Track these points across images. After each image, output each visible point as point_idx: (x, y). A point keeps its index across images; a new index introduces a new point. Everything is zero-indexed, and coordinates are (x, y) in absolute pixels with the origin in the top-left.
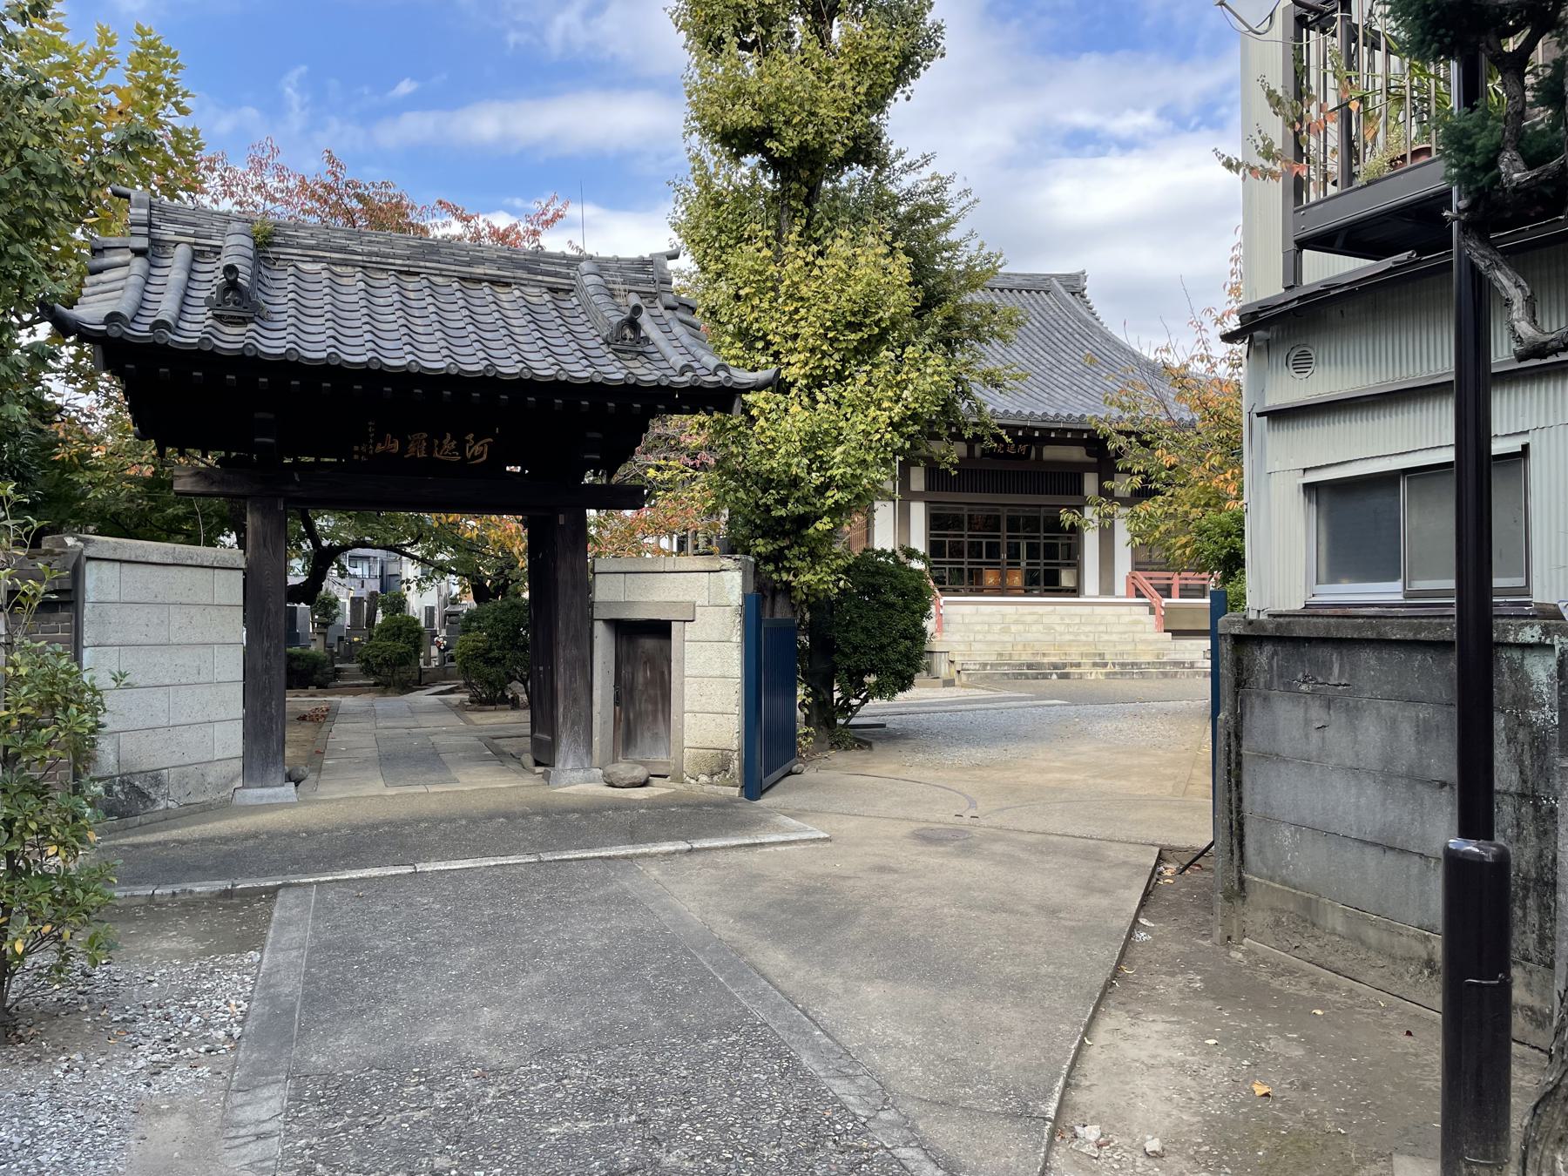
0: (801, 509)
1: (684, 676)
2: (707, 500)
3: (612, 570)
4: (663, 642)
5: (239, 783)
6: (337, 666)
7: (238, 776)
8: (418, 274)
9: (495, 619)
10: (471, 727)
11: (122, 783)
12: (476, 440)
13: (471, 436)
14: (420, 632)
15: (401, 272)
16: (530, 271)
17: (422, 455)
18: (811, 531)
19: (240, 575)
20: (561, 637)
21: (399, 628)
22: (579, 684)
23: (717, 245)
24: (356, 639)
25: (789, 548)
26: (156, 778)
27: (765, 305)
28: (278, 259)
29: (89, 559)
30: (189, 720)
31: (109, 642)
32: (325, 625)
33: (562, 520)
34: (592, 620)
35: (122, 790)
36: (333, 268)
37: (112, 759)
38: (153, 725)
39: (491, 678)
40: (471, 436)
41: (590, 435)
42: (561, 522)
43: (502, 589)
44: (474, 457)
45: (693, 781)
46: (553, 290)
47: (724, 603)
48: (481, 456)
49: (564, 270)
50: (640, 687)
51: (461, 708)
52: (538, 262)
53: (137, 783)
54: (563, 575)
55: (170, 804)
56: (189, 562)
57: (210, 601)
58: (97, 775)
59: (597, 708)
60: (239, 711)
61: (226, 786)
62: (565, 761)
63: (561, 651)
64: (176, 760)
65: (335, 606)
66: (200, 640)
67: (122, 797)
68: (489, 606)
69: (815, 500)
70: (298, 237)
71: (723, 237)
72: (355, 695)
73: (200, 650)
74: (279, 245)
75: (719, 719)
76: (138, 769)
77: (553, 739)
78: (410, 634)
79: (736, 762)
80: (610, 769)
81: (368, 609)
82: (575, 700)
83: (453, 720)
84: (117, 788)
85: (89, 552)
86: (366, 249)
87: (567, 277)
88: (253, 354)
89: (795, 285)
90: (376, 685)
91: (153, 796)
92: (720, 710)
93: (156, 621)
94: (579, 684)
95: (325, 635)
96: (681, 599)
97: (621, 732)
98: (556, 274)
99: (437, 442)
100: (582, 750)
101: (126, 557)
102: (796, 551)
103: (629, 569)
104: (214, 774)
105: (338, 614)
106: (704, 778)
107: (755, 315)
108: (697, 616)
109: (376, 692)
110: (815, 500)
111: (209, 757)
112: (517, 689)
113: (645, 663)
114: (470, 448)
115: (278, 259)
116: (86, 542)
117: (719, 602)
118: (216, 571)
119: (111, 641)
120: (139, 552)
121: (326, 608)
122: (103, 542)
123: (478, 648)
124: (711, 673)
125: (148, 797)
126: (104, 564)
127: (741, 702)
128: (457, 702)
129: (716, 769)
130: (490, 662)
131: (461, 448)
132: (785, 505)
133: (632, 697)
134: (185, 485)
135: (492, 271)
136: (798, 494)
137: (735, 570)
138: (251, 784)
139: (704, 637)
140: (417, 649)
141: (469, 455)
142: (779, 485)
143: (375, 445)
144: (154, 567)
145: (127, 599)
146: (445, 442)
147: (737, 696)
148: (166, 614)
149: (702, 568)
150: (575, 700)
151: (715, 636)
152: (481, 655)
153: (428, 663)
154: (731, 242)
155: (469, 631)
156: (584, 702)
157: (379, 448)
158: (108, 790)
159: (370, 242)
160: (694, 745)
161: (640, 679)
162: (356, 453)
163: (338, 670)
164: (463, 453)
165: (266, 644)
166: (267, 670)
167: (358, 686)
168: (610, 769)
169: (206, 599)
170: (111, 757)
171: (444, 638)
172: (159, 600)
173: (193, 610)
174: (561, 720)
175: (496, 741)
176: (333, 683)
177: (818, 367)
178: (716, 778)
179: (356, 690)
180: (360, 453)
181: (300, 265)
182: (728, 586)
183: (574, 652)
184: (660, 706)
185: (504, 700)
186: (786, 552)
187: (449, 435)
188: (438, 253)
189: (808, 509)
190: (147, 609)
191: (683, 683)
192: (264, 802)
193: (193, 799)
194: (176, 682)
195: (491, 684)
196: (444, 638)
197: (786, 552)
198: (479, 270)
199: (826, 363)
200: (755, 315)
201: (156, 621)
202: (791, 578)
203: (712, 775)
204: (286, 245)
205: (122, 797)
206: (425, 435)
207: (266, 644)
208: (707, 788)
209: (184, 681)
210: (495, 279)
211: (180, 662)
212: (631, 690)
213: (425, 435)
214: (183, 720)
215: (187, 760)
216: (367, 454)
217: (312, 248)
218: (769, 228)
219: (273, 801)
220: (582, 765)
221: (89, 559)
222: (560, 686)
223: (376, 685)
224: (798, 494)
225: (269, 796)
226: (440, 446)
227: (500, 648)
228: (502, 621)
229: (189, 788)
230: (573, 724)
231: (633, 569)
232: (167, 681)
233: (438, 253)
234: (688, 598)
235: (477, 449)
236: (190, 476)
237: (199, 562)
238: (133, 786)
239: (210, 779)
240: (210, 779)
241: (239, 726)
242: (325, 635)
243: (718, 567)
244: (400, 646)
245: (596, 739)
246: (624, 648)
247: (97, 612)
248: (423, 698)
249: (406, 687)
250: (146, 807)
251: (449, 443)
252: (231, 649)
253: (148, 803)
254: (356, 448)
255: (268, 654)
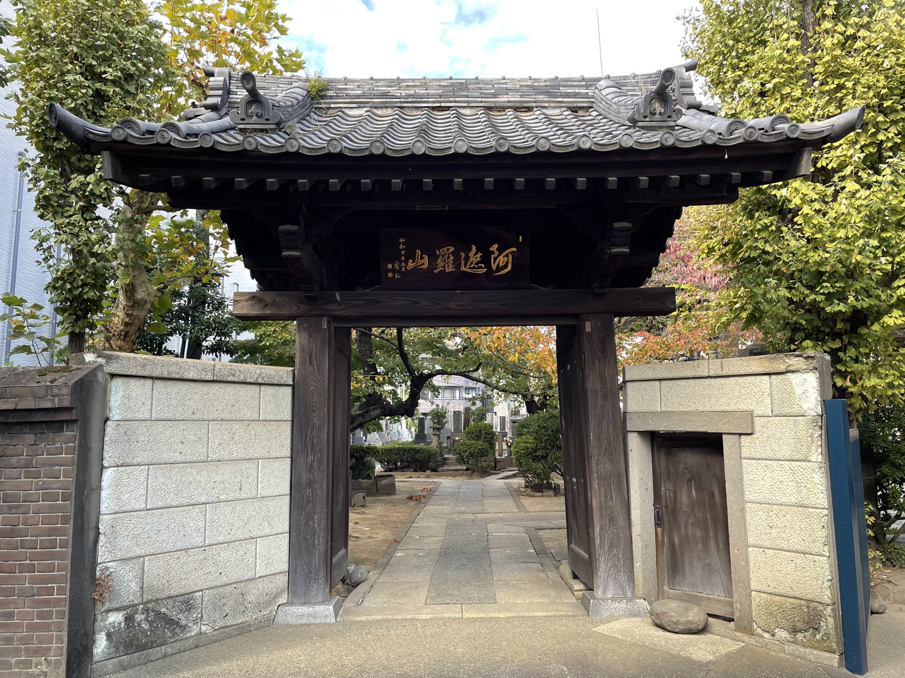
0: (865, 303)
1: (744, 502)
2: (722, 316)
3: (645, 377)
4: (712, 460)
5: (283, 599)
6: (446, 456)
7: (283, 591)
8: (448, 108)
9: (539, 426)
10: (522, 514)
11: (146, 611)
12: (501, 251)
13: (496, 246)
14: (493, 434)
15: (434, 108)
16: (549, 94)
17: (450, 269)
18: (876, 327)
19: (289, 390)
20: (594, 449)
21: (480, 431)
22: (616, 502)
23: (734, 54)
24: (457, 438)
25: (844, 349)
26: (187, 602)
27: (798, 93)
28: (329, 108)
29: (113, 376)
30: (228, 538)
31: (135, 462)
32: (439, 429)
33: (588, 327)
34: (625, 433)
35: (146, 620)
36: (376, 111)
37: (134, 586)
38: (186, 545)
39: (538, 471)
40: (496, 246)
41: (617, 225)
42: (588, 329)
43: (544, 405)
44: (499, 269)
45: (766, 635)
46: (574, 110)
47: (795, 411)
48: (506, 266)
49: (583, 91)
50: (685, 509)
51: (516, 493)
52: (558, 87)
53: (163, 610)
54: (592, 384)
55: (204, 628)
56: (230, 379)
57: (255, 417)
58: (115, 605)
59: (636, 530)
60: (283, 524)
61: (269, 603)
62: (605, 589)
63: (594, 465)
64: (212, 580)
65: (445, 417)
66: (242, 455)
67: (145, 626)
68: (536, 415)
69: (879, 292)
70: (347, 89)
71: (740, 45)
72: (454, 476)
73: (246, 465)
74: (331, 97)
75: (799, 559)
76: (167, 593)
77: (590, 557)
78: (488, 436)
79: (831, 620)
80: (659, 607)
81: (465, 418)
82: (612, 520)
83: (509, 505)
84: (139, 617)
85: (114, 368)
86: (404, 93)
87: (586, 96)
88: (253, 147)
89: (835, 59)
90: (467, 469)
91: (183, 622)
92: (799, 548)
93: (192, 438)
94: (616, 502)
95: (438, 435)
96: (732, 407)
97: (665, 556)
98: (575, 95)
99: (463, 255)
100: (623, 577)
101: (156, 373)
102: (852, 352)
103: (665, 376)
104: (254, 593)
105: (446, 422)
106: (782, 634)
107: (786, 105)
108: (757, 428)
109: (467, 475)
110: (879, 292)
111: (250, 575)
112: (557, 480)
113: (689, 481)
114: (495, 259)
115: (329, 108)
116: (109, 358)
117: (787, 410)
118: (263, 388)
119: (139, 460)
120: (173, 368)
121: (439, 418)
122: (129, 359)
123: (528, 448)
124: (784, 500)
125: (178, 623)
126: (133, 381)
127: (832, 540)
128: (515, 487)
129: (800, 625)
130: (536, 459)
131: (486, 259)
132: (844, 299)
133: (675, 520)
134: (242, 308)
135: (515, 98)
136: (858, 286)
137: (806, 371)
138: (295, 600)
139: (768, 454)
140: (492, 446)
141: (494, 267)
142: (833, 276)
143: (406, 262)
144: (192, 384)
145: (161, 416)
146: (471, 254)
147: (824, 533)
148: (204, 431)
149: (761, 370)
150: (612, 520)
151: (786, 453)
152: (530, 454)
153: (500, 455)
154: (749, 49)
155: (522, 435)
156: (621, 522)
157: (411, 265)
158: (129, 619)
159: (408, 86)
160: (765, 588)
161: (684, 499)
162: (390, 271)
163: (445, 459)
164: (488, 265)
165: (310, 458)
166: (310, 483)
167: (456, 470)
168: (659, 607)
169: (249, 414)
170: (133, 585)
171: (510, 438)
172: (196, 417)
173: (236, 426)
174: (597, 542)
175: (540, 533)
176: (441, 468)
177: (871, 144)
178: (800, 636)
179: (455, 473)
180: (393, 271)
181: (347, 111)
182: (799, 391)
183: (608, 466)
184: (711, 534)
185: (549, 486)
186: (841, 354)
187: (474, 248)
188: (466, 89)
189: (873, 302)
190: (182, 426)
191: (743, 510)
192: (304, 621)
193: (230, 621)
194: (214, 499)
195: (538, 475)
196: (510, 438)
197: (841, 354)
198: (503, 99)
199: (881, 137)
200: (786, 105)
201: (192, 438)
202: (848, 383)
203: (794, 631)
204: (337, 97)
205: (145, 626)
206: (452, 249)
207: (310, 458)
208: (790, 648)
209: (222, 497)
210: (518, 105)
211: (218, 479)
212: (674, 512)
213: (452, 249)
214: (221, 539)
215: (224, 580)
216: (399, 272)
217: (358, 97)
218: (793, 19)
219: (313, 621)
220: (625, 594)
221: (113, 376)
222: (595, 504)
223: (467, 469)
224: (858, 286)
225: (309, 615)
226: (467, 259)
227: (545, 448)
228: (544, 427)
229: (227, 609)
230: (612, 546)
231: (670, 376)
232: (204, 499)
233: (466, 89)
234: (742, 407)
235: (502, 260)
236: (247, 300)
237: (242, 378)
238: (158, 613)
239: (251, 598)
240: (251, 598)
241: (285, 540)
242: (438, 435)
243: (782, 368)
244: (481, 444)
245: (638, 565)
246: (663, 463)
247: (122, 430)
248: (494, 482)
249: (485, 472)
250: (174, 634)
251: (475, 256)
252: (277, 463)
253: (178, 630)
254: (390, 266)
255: (311, 467)
